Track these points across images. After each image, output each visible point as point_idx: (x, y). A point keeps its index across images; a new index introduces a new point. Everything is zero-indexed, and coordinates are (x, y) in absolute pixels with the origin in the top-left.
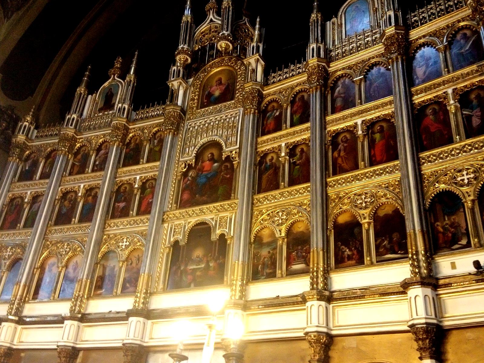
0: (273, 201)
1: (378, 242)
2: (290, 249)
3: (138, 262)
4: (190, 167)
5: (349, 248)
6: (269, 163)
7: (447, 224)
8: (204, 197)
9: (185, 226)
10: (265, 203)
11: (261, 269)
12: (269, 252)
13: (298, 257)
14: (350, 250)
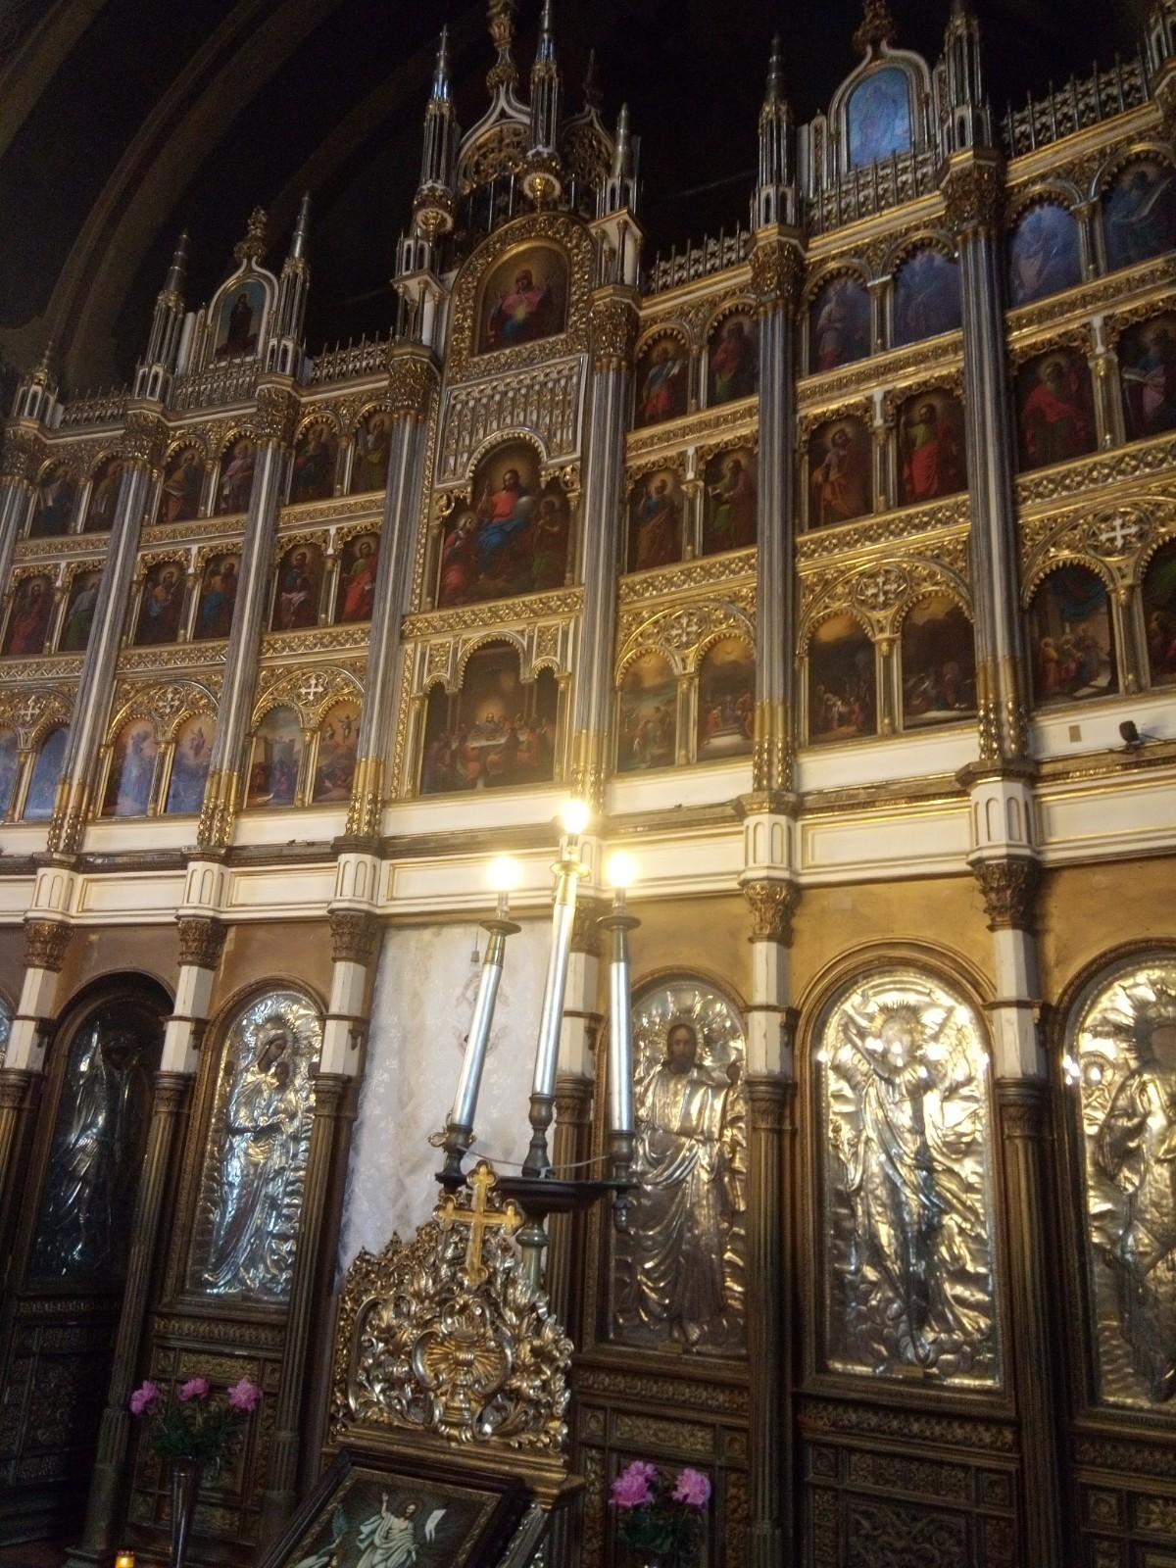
4: (460, 506)
6: (655, 497)
7: (1067, 642)
9: (456, 650)
12: (658, 709)
14: (845, 702)
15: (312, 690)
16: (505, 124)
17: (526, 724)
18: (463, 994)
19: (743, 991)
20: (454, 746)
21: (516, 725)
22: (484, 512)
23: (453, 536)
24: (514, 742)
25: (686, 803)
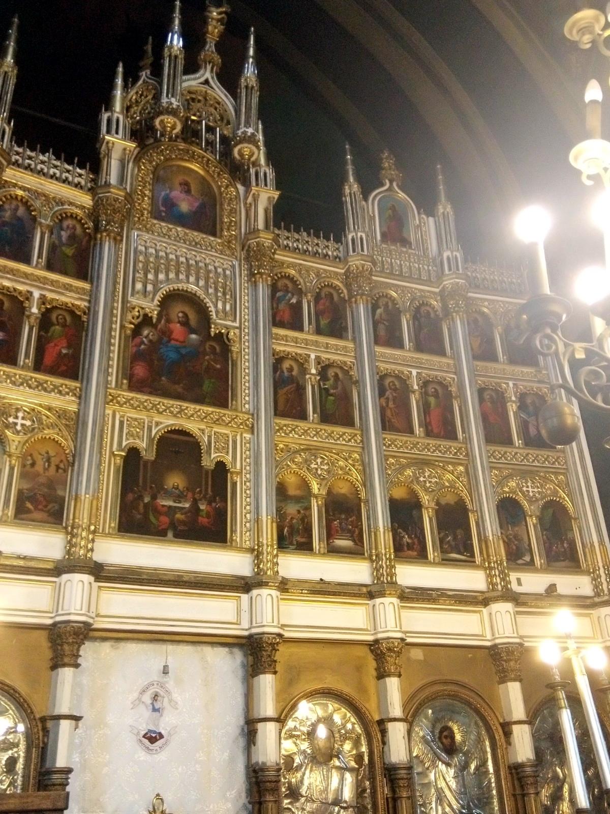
0: (303, 437)
1: (442, 535)
2: (330, 515)
3: (49, 466)
4: (146, 320)
5: (407, 534)
6: (286, 374)
7: (511, 535)
8: (177, 386)
9: (150, 429)
10: (291, 435)
11: (289, 534)
12: (299, 512)
13: (343, 530)
14: (410, 537)
15: (530, 489)
16: (204, 88)
17: (205, 497)
18: (139, 699)
19: (322, 707)
20: (147, 500)
21: (197, 496)
22: (163, 333)
23: (137, 340)
24: (195, 510)
25: (327, 578)
